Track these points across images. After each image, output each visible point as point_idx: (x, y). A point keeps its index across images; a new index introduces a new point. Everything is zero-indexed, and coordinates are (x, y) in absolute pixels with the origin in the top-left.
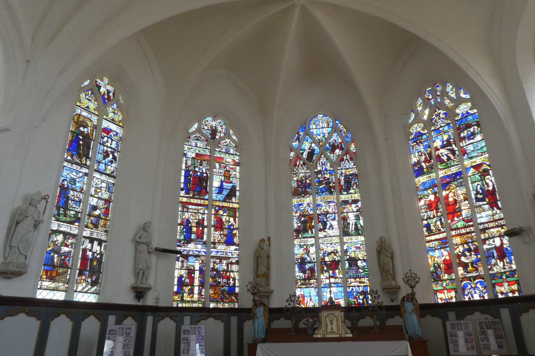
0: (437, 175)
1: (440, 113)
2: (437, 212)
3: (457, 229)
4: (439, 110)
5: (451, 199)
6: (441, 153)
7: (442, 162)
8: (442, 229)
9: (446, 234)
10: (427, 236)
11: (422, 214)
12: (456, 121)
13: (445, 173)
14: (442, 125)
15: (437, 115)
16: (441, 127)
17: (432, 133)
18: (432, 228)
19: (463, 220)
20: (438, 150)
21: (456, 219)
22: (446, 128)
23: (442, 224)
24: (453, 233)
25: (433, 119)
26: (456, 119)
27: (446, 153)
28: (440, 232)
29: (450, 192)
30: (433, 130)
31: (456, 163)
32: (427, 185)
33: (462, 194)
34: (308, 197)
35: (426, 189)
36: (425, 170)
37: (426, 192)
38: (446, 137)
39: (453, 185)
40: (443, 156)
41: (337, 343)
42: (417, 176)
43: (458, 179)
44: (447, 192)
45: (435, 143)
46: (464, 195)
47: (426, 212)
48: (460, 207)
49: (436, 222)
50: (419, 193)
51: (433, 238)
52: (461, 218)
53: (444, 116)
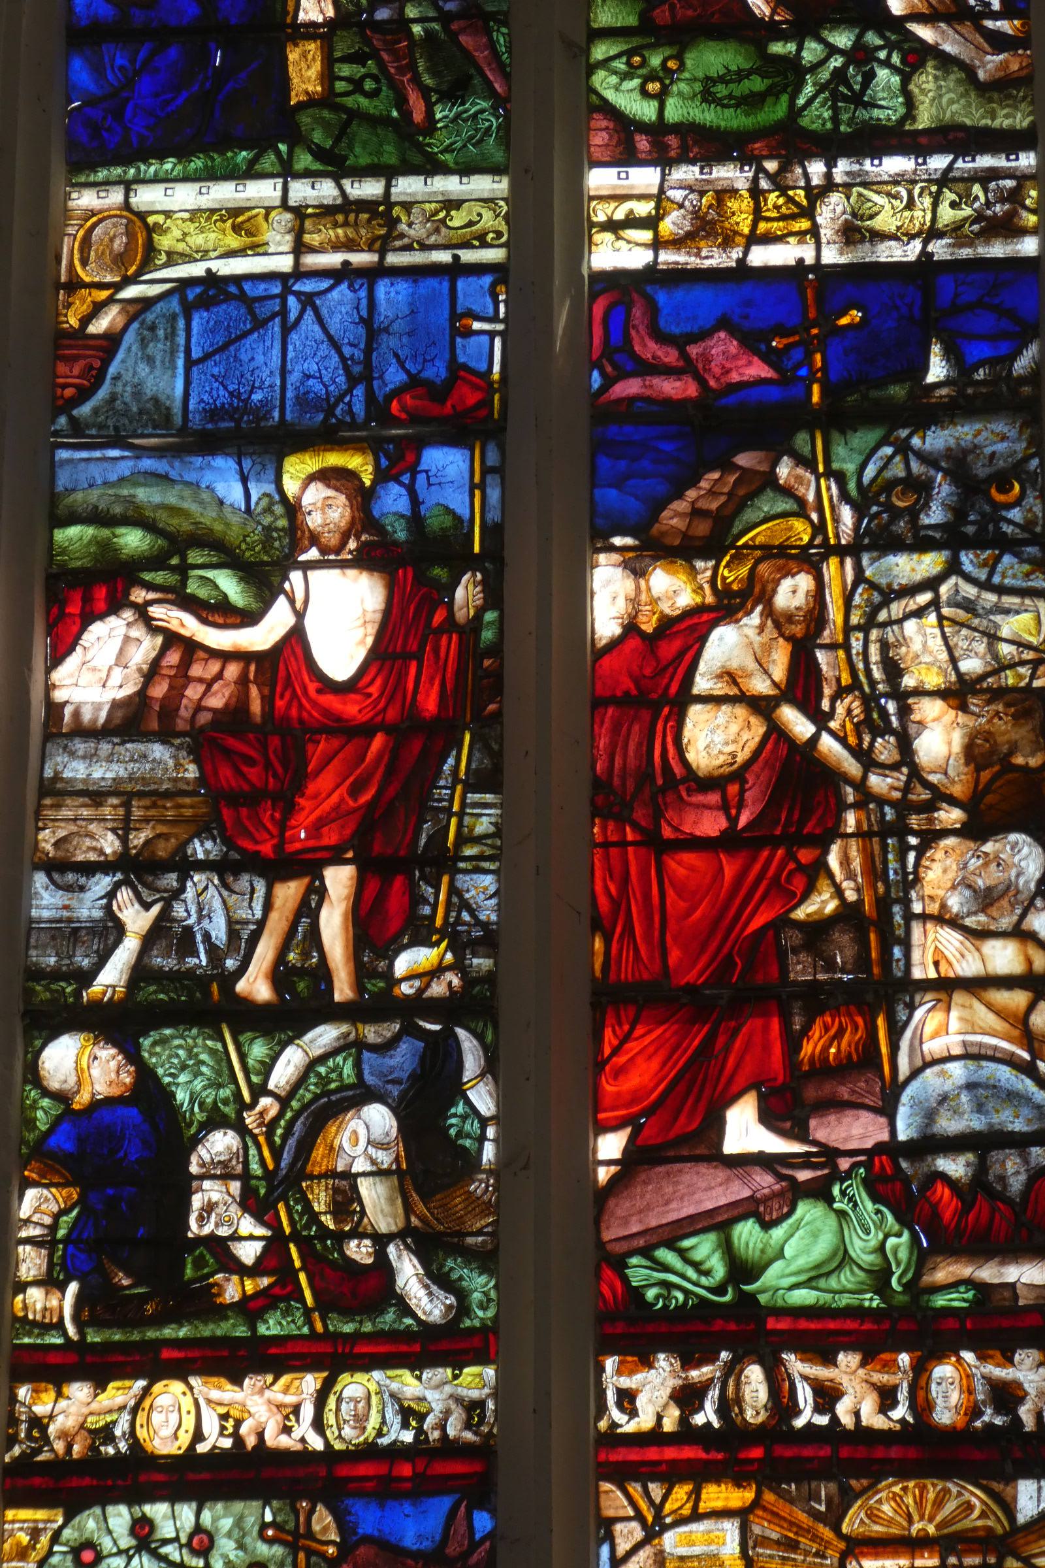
0: (547, 219)
2: (373, 935)
3: (734, 1324)
5: (713, 738)
8: (408, 1272)
9: (478, 1380)
10: (56, 1368)
11: (46, 900)
13: (707, 227)
18: (213, 1207)
19: (892, 1176)
21: (744, 1129)
23: (429, 1158)
24: (647, 1395)
28: (348, 1323)
29: (727, 606)
31: (935, 100)
32: (295, 362)
33: (958, 693)
34: (646, 1183)
35: (259, 437)
36: (305, 71)
37: (225, 488)
39: (816, 490)
41: (117, 650)
42: (116, 138)
43: (927, 411)
44: (673, 589)
46: (982, 714)
47: (135, 869)
48: (880, 921)
49: (325, 1106)
50: (90, 472)
51: (177, 1415)
52: (857, 1131)
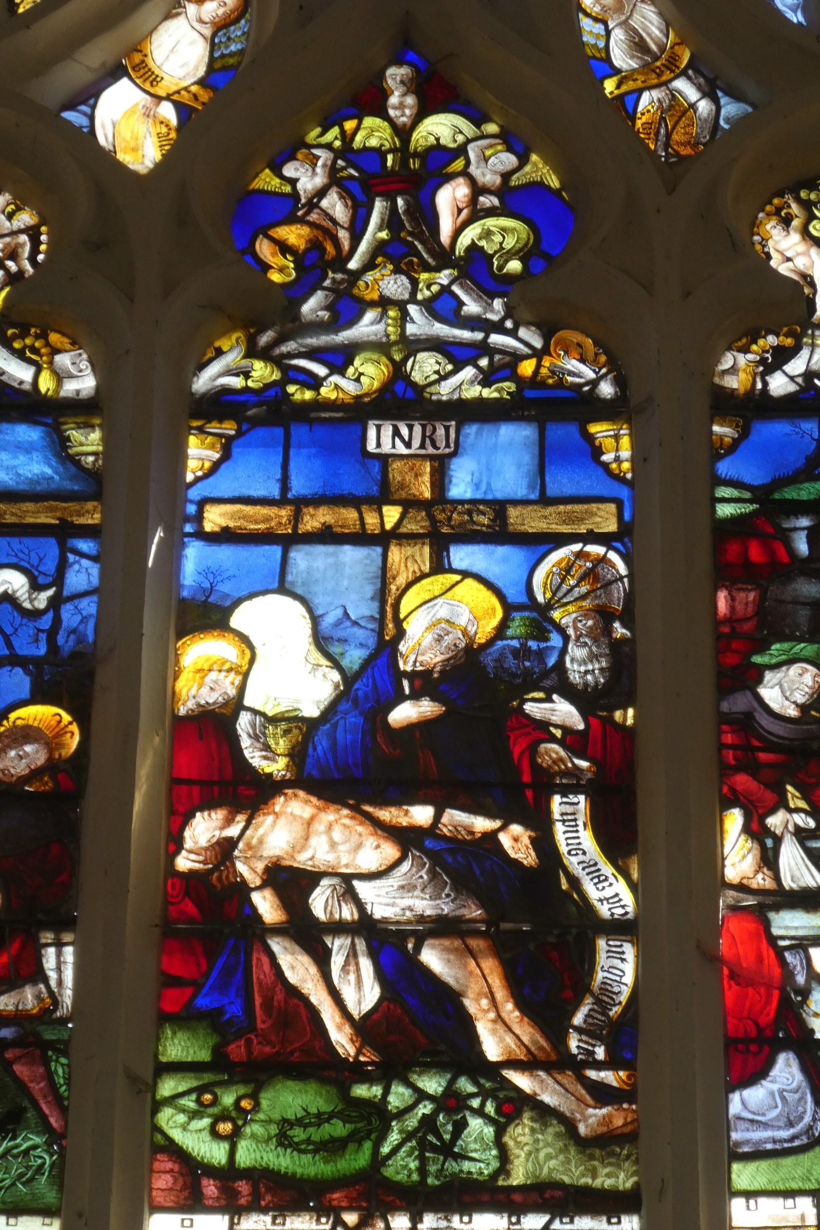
1: (439, 163)
4: (432, 96)
6: (291, 882)
7: (269, 1042)
12: (724, 404)
14: (424, 367)
15: (363, 176)
16: (399, 399)
17: (199, 453)
20: (249, 794)
22: (493, 464)
25: (290, 207)
26: (736, 369)
27: (386, 901)
30: (220, 404)
38: (449, 612)
40: (311, 936)
45: (201, 652)
53: (504, 234)
